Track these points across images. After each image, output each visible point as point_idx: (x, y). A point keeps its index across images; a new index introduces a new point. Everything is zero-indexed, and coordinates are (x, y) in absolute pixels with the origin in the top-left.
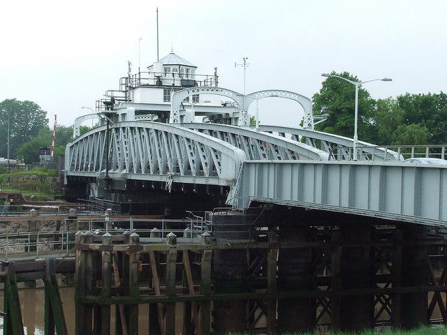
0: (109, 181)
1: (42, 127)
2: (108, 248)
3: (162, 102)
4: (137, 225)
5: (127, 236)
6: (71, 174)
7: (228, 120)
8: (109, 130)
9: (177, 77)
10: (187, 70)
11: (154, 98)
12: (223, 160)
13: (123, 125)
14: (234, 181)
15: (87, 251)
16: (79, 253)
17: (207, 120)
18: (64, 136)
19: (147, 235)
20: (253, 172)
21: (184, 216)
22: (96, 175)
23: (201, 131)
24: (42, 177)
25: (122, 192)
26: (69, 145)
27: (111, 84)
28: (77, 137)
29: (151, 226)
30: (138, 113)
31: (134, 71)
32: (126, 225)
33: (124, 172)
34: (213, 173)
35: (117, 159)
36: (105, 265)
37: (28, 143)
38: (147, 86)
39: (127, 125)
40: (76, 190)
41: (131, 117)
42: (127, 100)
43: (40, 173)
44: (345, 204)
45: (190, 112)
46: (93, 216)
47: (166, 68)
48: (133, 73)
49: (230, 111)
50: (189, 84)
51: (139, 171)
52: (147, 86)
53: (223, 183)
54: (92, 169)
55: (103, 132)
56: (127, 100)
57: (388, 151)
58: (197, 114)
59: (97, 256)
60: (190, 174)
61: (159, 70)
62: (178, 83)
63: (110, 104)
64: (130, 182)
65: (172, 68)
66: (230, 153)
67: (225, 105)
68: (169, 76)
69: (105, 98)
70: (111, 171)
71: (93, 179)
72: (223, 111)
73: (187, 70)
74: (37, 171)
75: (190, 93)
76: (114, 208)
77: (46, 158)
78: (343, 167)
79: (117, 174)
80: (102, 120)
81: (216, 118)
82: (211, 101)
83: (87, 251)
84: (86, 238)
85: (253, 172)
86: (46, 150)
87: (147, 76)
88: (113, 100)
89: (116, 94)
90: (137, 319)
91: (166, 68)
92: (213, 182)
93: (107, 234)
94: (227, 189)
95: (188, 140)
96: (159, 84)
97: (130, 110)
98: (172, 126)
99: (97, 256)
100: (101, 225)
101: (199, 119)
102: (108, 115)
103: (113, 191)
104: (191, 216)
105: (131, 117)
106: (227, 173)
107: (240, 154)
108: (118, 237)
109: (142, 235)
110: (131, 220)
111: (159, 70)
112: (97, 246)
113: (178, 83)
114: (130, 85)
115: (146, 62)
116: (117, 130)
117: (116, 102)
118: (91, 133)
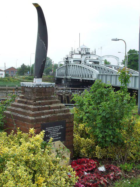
0: (67, 79)
1: (71, 159)
2: (64, 95)
3: (80, 58)
4: (71, 90)
5: (69, 92)
6: (57, 77)
7: (98, 63)
8: (67, 65)
9: (85, 51)
10: (87, 50)
11: (78, 57)
12: (94, 73)
13: (70, 64)
14: (96, 79)
15: (59, 96)
16: (57, 96)
17: (93, 63)
18: (56, 66)
19: (74, 92)
20: (100, 77)
21: (84, 87)
22: (64, 77)
23: (88, 66)
24: (50, 78)
25: (70, 82)
26: (57, 69)
27: (67, 53)
28: (59, 67)
29: (75, 90)
30: (74, 61)
31: (73, 50)
32: (69, 90)
33: (70, 76)
34: (91, 77)
35: (69, 73)
36: (64, 99)
37: (47, 69)
38: (77, 54)
39: (71, 64)
40: (59, 81)
41: (72, 62)
42: (71, 58)
43: (49, 77)
44: (133, 86)
45: (88, 61)
46: (62, 88)
47: (82, 49)
48: (73, 50)
49: (98, 61)
50: (88, 53)
51: (76, 76)
52: (77, 54)
53: (93, 80)
54: (62, 76)
55: (65, 66)
56: (71, 58)
57: (137, 72)
58: (90, 61)
59: (62, 96)
60: (89, 77)
61: (80, 50)
62: (85, 53)
63: (67, 59)
64: (72, 79)
65: (83, 49)
66: (95, 72)
67: (97, 59)
68: (83, 51)
69: (76, 49)
70: (67, 76)
71: (63, 78)
72: (97, 61)
73: (87, 50)
74: (49, 76)
75: (88, 56)
76: (68, 86)
77: (51, 73)
78: (137, 77)
79: (69, 77)
80: (65, 63)
81: (95, 63)
82: (94, 58)
83: (59, 96)
84: (59, 92)
85: (100, 77)
86: (51, 70)
87: (77, 51)
88: (68, 57)
89: (68, 56)
90: (101, 171)
91: (82, 49)
92: (91, 79)
93: (64, 91)
94: (94, 81)
95: (86, 68)
96: (80, 53)
97: (72, 60)
98: (83, 65)
99: (62, 96)
100: (63, 90)
101: (91, 63)
102: (67, 62)
103: (68, 82)
104: (85, 88)
105: (72, 62)
106: (94, 77)
107: (97, 72)
108: (67, 92)
109: (72, 92)
110: (70, 88)
111: (80, 50)
112: (62, 94)
113: (85, 53)
114: (72, 54)
115: (76, 48)
116: (69, 65)
117: (69, 58)
118: (64, 66)
